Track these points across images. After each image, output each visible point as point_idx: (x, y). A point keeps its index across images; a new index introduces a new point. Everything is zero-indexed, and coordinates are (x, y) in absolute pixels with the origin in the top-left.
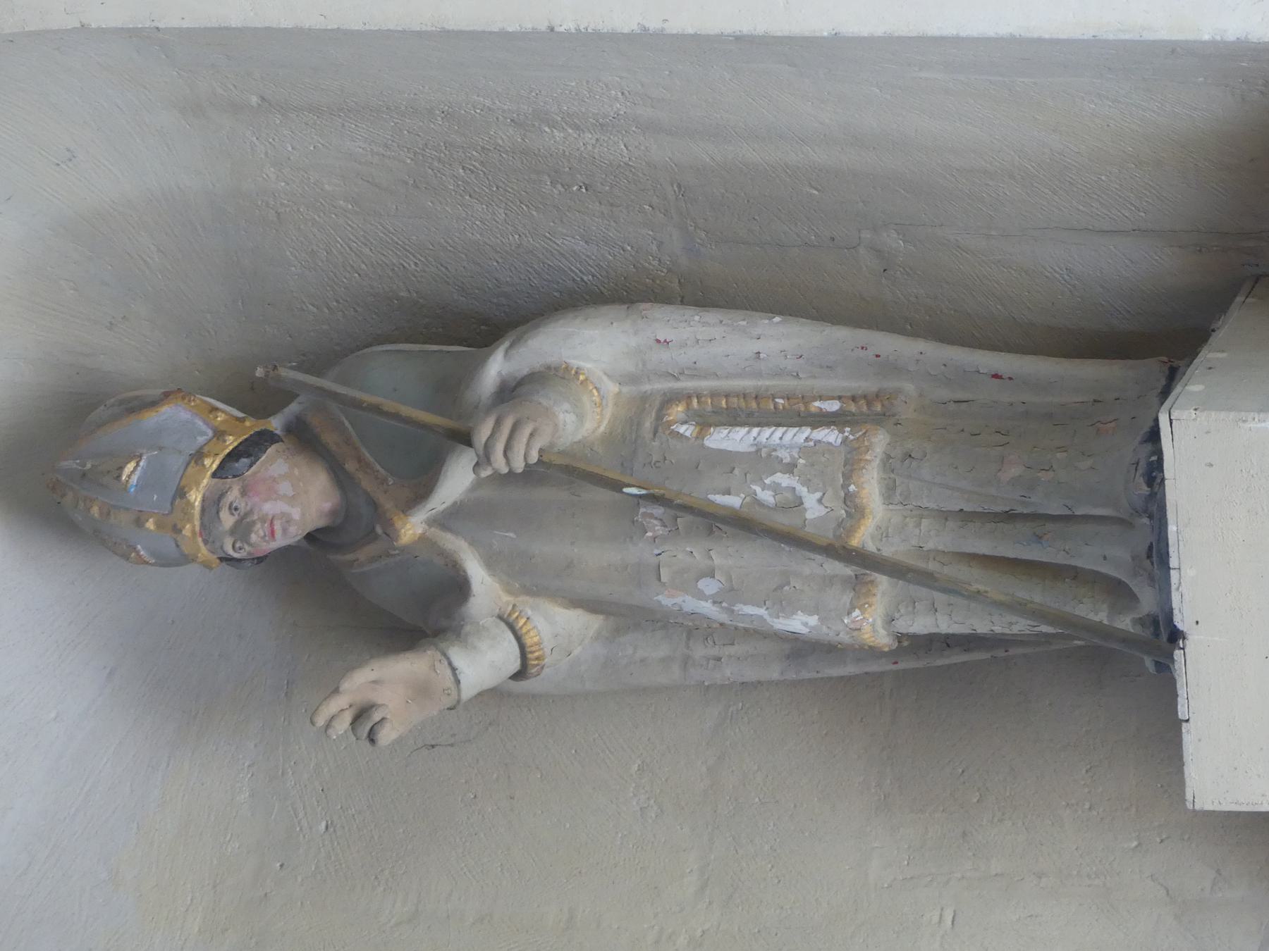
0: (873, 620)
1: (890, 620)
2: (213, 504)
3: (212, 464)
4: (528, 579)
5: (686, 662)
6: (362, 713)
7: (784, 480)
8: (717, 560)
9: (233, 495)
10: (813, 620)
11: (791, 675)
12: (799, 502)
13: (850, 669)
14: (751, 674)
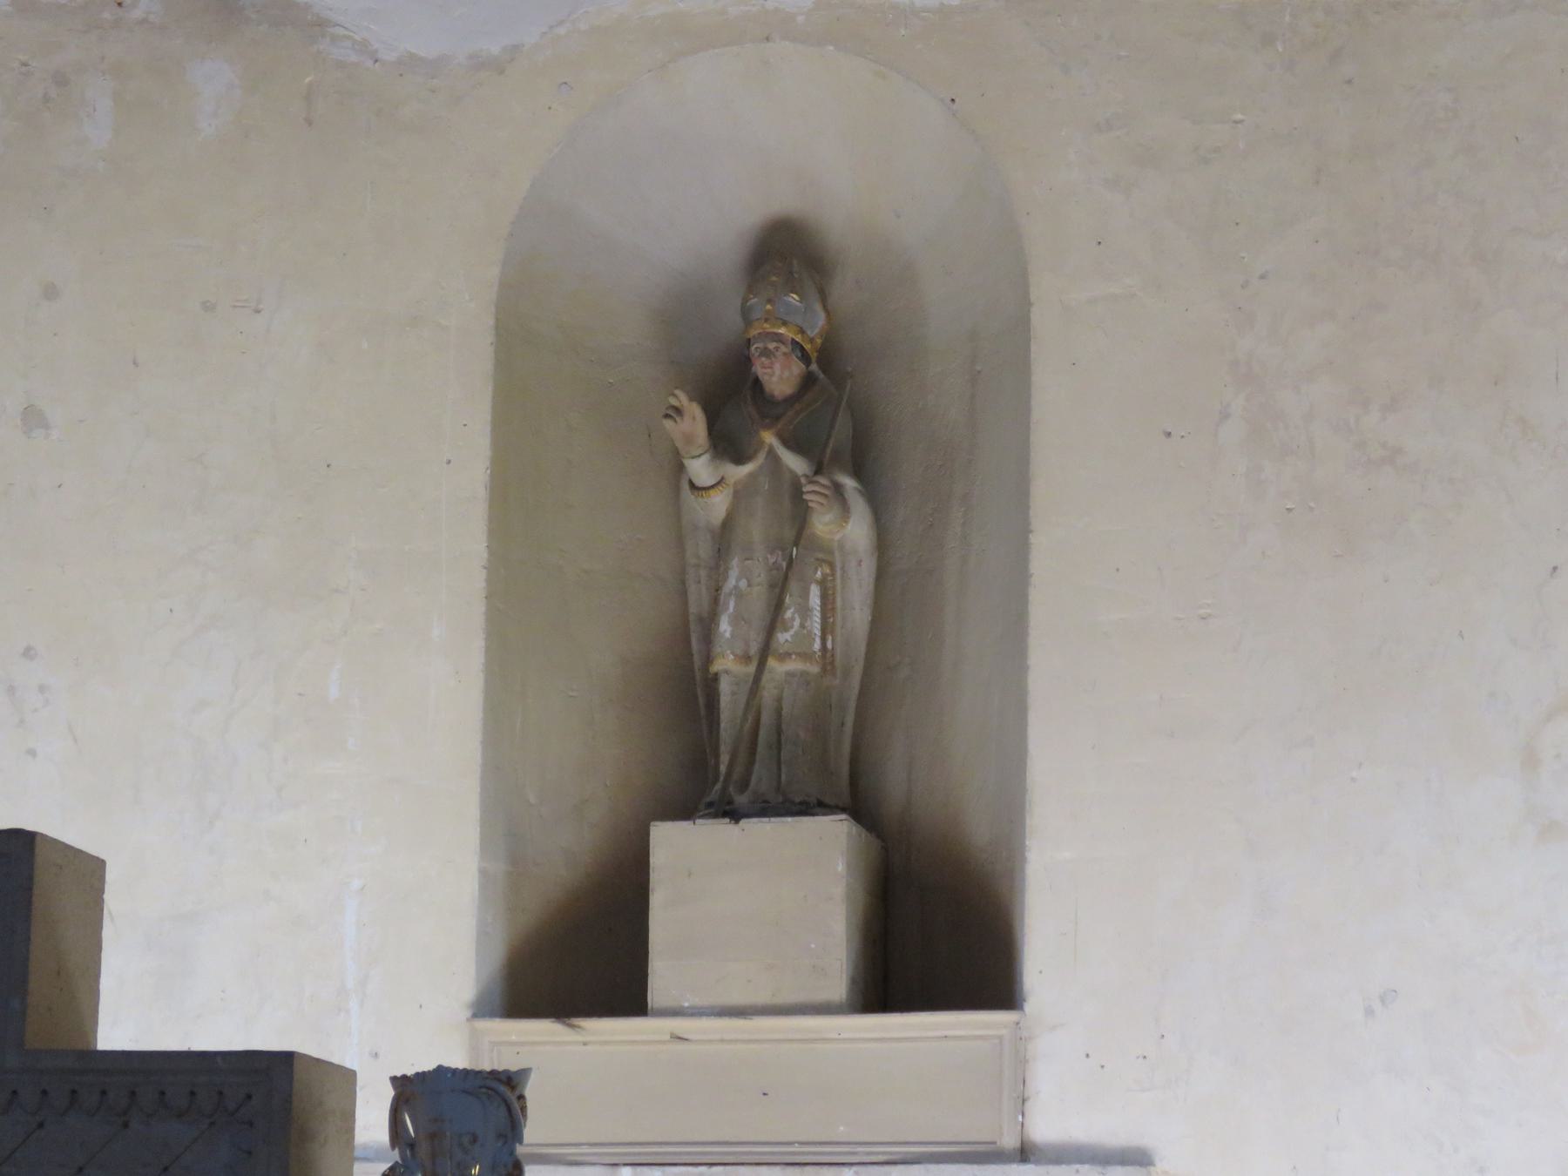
0: (728, 665)
1: (727, 672)
2: (779, 338)
3: (798, 338)
4: (741, 494)
5: (697, 566)
6: (678, 411)
7: (797, 623)
8: (756, 589)
9: (783, 349)
10: (728, 635)
11: (691, 618)
12: (786, 630)
13: (695, 645)
14: (692, 598)
